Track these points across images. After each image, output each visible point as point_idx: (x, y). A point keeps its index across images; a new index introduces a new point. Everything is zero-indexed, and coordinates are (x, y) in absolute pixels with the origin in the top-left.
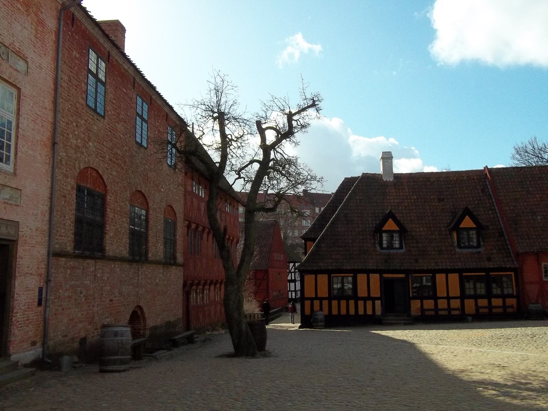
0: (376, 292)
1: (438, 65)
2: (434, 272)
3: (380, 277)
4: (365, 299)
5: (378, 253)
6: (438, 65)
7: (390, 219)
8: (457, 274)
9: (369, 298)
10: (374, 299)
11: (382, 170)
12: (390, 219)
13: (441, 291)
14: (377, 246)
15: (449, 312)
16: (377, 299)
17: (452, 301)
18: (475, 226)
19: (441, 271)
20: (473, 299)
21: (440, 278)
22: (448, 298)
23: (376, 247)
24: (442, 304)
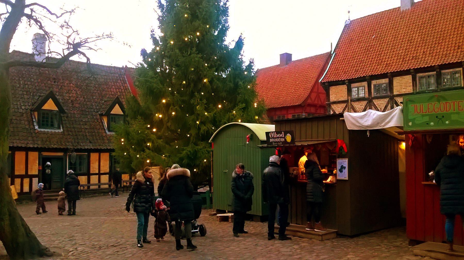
0: (34, 170)
1: (163, 34)
2: (90, 151)
3: (39, 155)
4: (22, 177)
5: (36, 131)
6: (163, 34)
7: (50, 99)
8: (37, 178)
9: (27, 175)
10: (31, 177)
11: (347, 177)
12: (50, 99)
13: (94, 168)
14: (35, 124)
15: (99, 186)
16: (35, 176)
17: (102, 177)
18: (44, 108)
19: (95, 151)
20: (76, 201)
21: (94, 157)
22: (99, 174)
23: (34, 126)
24: (94, 179)
